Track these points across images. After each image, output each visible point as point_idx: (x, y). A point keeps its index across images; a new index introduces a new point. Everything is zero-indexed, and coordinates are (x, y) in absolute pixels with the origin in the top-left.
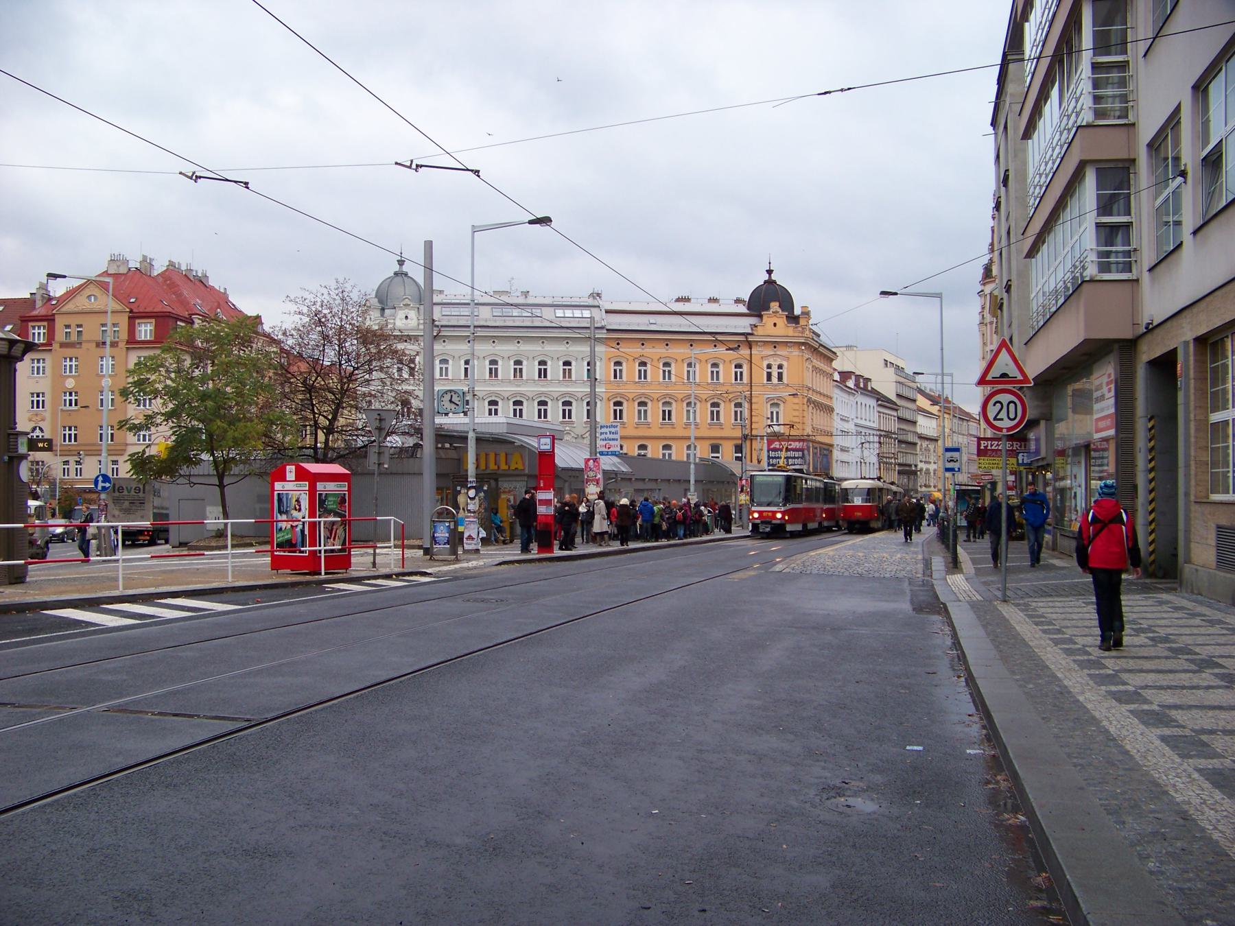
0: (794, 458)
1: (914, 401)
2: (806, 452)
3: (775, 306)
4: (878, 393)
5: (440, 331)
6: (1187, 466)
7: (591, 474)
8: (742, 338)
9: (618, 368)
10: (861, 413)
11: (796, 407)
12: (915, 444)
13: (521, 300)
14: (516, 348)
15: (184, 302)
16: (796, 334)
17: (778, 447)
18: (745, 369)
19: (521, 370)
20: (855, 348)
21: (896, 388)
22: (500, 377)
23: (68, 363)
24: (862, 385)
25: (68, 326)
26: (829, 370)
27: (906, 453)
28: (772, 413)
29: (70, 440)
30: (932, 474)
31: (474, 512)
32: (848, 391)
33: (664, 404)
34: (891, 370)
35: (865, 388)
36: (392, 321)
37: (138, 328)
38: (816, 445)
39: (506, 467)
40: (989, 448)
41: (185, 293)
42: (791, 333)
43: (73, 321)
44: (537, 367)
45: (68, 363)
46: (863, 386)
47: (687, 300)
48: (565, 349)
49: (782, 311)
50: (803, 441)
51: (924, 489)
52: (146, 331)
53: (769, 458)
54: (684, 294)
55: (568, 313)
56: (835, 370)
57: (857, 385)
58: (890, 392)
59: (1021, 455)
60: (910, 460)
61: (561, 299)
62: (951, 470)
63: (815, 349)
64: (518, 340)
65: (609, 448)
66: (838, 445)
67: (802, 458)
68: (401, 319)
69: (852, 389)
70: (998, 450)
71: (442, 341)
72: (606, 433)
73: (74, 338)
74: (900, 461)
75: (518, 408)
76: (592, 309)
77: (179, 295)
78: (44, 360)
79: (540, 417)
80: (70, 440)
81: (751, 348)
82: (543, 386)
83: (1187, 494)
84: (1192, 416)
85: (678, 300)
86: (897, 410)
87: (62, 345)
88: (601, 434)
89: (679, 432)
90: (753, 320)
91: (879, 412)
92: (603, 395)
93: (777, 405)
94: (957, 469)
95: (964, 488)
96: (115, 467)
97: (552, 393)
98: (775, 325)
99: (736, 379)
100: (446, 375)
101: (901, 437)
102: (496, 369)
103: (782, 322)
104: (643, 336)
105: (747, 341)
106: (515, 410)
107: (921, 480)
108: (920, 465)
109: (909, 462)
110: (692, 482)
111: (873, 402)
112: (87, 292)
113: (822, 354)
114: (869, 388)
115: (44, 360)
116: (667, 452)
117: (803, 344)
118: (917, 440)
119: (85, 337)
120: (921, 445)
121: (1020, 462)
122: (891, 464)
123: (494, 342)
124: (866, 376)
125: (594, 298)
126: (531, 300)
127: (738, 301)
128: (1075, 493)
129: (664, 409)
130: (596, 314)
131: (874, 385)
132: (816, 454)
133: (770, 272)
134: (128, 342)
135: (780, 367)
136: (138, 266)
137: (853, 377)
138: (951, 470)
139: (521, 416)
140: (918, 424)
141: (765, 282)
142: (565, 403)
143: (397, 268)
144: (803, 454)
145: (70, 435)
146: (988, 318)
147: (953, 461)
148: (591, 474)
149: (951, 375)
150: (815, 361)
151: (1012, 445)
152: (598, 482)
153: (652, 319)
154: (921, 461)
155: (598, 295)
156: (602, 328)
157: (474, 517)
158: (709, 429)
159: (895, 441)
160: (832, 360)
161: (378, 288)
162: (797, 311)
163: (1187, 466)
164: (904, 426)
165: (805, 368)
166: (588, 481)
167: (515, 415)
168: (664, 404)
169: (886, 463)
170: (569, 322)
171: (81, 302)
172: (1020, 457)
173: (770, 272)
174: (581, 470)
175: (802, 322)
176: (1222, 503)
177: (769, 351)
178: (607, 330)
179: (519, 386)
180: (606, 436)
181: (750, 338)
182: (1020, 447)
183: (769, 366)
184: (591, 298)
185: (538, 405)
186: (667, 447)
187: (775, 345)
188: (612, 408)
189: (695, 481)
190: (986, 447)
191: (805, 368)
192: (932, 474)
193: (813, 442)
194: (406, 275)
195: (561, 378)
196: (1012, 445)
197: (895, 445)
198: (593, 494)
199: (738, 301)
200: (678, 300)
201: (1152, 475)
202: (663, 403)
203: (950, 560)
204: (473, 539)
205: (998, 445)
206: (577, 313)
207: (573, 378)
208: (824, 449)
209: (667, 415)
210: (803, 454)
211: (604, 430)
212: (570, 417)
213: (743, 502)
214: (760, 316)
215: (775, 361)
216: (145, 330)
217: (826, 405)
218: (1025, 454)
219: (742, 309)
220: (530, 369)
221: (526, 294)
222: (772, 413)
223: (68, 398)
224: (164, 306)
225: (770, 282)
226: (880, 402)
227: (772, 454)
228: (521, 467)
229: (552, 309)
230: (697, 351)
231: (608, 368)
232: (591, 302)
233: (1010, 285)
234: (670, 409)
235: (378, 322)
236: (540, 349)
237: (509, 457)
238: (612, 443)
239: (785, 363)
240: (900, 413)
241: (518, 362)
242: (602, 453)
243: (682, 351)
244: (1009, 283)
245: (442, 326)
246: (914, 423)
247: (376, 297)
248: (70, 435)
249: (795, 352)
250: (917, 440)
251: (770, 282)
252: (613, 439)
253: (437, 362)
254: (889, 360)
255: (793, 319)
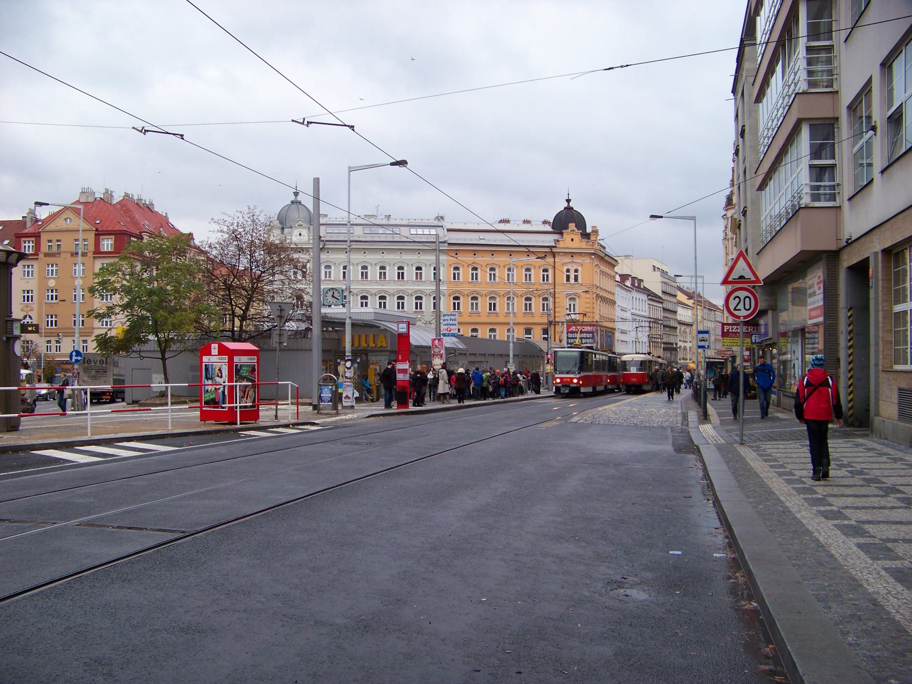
0: (587, 338)
1: (675, 296)
2: (595, 334)
3: (572, 226)
4: (649, 290)
5: (325, 245)
6: (877, 344)
7: (437, 350)
8: (548, 250)
9: (456, 272)
10: (636, 305)
11: (588, 301)
12: (676, 328)
13: (385, 222)
14: (381, 257)
15: (136, 223)
16: (588, 247)
17: (574, 330)
18: (550, 273)
19: (385, 273)
20: (631, 257)
21: (662, 286)
22: (369, 279)
23: (50, 268)
24: (636, 285)
25: (50, 241)
26: (612, 273)
27: (669, 335)
28: (570, 305)
29: (52, 325)
30: (688, 350)
31: (350, 378)
32: (626, 289)
33: (490, 298)
34: (658, 274)
35: (639, 287)
36: (290, 237)
37: (102, 243)
38: (603, 329)
39: (374, 345)
40: (730, 331)
41: (137, 216)
42: (584, 246)
43: (54, 237)
44: (396, 271)
45: (50, 268)
46: (638, 285)
47: (507, 221)
48: (417, 258)
49: (578, 229)
50: (593, 325)
51: (682, 361)
52: (108, 244)
53: (568, 338)
54: (505, 217)
55: (420, 231)
56: (617, 273)
57: (633, 284)
58: (657, 289)
59: (754, 336)
60: (672, 340)
61: (414, 221)
62: (703, 347)
63: (602, 258)
64: (383, 251)
65: (450, 331)
66: (619, 329)
67: (592, 338)
68: (296, 236)
69: (629, 287)
70: (737, 332)
71: (326, 252)
72: (448, 320)
73: (55, 249)
74: (665, 340)
75: (382, 301)
76: (437, 228)
77: (132, 218)
78: (32, 266)
79: (398, 308)
80: (52, 325)
81: (554, 257)
82: (401, 285)
83: (876, 365)
84: (880, 307)
85: (501, 222)
86: (662, 303)
87: (46, 255)
88: (444, 320)
89: (502, 319)
90: (556, 237)
91: (649, 304)
92: (445, 292)
93: (574, 299)
94: (706, 347)
95: (712, 360)
96: (85, 345)
97: (408, 291)
98: (572, 240)
99: (544, 280)
100: (330, 277)
101: (665, 323)
102: (366, 273)
103: (577, 238)
104: (475, 249)
105: (551, 252)
106: (380, 303)
107: (680, 355)
108: (680, 344)
109: (671, 341)
110: (511, 356)
111: (644, 297)
112: (64, 216)
113: (607, 262)
114: (642, 287)
115: (32, 266)
116: (493, 334)
117: (593, 254)
118: (677, 325)
119: (62, 249)
120: (680, 329)
121: (754, 341)
122: (658, 342)
123: (365, 253)
124: (640, 278)
125: (439, 220)
126: (392, 222)
127: (545, 222)
128: (794, 364)
129: (491, 302)
130: (440, 232)
131: (646, 284)
132: (602, 335)
133: (568, 201)
134: (94, 253)
135: (576, 271)
136: (102, 196)
137: (630, 279)
138: (703, 347)
139: (385, 307)
140: (678, 313)
141: (565, 208)
142: (417, 298)
143: (293, 198)
144: (593, 335)
145: (52, 321)
146: (730, 235)
147: (703, 340)
148: (437, 350)
149: (703, 277)
150: (602, 266)
151: (747, 329)
152: (441, 356)
153: (482, 235)
154: (680, 341)
155: (442, 218)
156: (445, 242)
157: (350, 382)
158: (524, 317)
159: (661, 325)
160: (615, 266)
161: (279, 213)
162: (589, 230)
163: (877, 344)
164: (667, 315)
165: (594, 272)
166: (434, 355)
167: (380, 307)
168: (490, 298)
169: (655, 342)
170: (420, 238)
171: (60, 223)
172: (753, 338)
173: (568, 201)
174: (429, 347)
175: (592, 238)
176: (902, 372)
177: (568, 259)
178: (449, 244)
179: (383, 285)
180: (448, 322)
181: (554, 250)
182: (754, 330)
183: (568, 271)
184: (437, 220)
185: (398, 299)
186: (492, 330)
187: (572, 255)
188: (452, 301)
189: (514, 355)
190: (728, 330)
191: (594, 272)
192: (688, 350)
193: (601, 326)
194: (300, 203)
195: (414, 280)
196: (747, 329)
197: (661, 328)
198: (438, 365)
199: (545, 222)
200: (501, 222)
201: (851, 351)
202: (490, 298)
203: (702, 413)
204: (349, 398)
205: (737, 329)
206: (426, 231)
207: (423, 279)
208: (609, 332)
209: (492, 307)
210: (593, 335)
211: (446, 318)
212: (421, 308)
213: (549, 371)
214: (561, 234)
215: (572, 266)
216: (107, 244)
217: (610, 299)
218: (757, 336)
219: (548, 228)
220: (392, 273)
221: (388, 217)
222: (570, 305)
223: (50, 294)
224: (121, 226)
225: (569, 209)
226: (650, 297)
227: (570, 335)
228: (384, 345)
229: (407, 228)
230: (515, 259)
231: (449, 272)
232: (436, 223)
233: (746, 211)
234: (494, 302)
235: (279, 238)
236: (399, 257)
237: (376, 337)
238: (452, 327)
239: (580, 268)
240: (665, 305)
241: (383, 268)
242: (444, 335)
243: (504, 259)
244: (745, 209)
245: (326, 241)
246: (675, 312)
247: (278, 219)
248: (52, 321)
249: (587, 260)
250: (677, 325)
251: (569, 209)
252: (453, 325)
253: (323, 267)
254: (656, 266)
255: (586, 236)
